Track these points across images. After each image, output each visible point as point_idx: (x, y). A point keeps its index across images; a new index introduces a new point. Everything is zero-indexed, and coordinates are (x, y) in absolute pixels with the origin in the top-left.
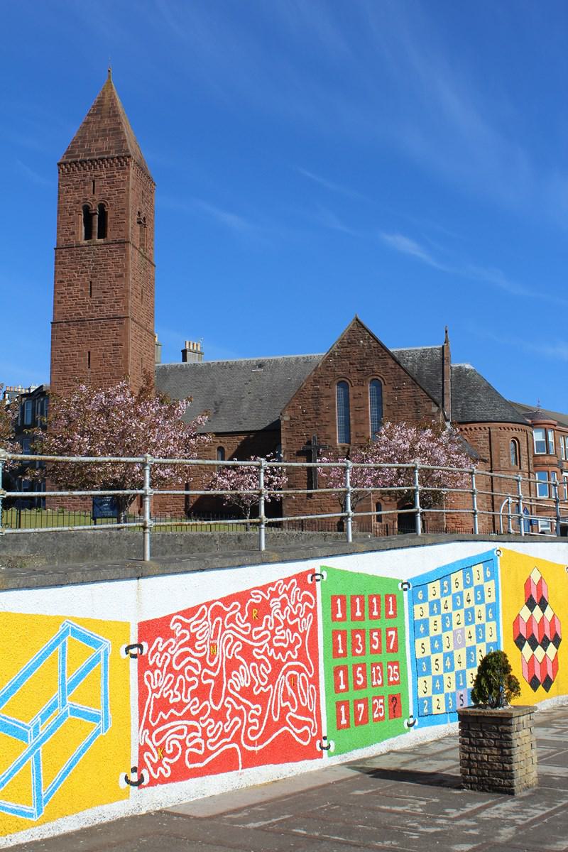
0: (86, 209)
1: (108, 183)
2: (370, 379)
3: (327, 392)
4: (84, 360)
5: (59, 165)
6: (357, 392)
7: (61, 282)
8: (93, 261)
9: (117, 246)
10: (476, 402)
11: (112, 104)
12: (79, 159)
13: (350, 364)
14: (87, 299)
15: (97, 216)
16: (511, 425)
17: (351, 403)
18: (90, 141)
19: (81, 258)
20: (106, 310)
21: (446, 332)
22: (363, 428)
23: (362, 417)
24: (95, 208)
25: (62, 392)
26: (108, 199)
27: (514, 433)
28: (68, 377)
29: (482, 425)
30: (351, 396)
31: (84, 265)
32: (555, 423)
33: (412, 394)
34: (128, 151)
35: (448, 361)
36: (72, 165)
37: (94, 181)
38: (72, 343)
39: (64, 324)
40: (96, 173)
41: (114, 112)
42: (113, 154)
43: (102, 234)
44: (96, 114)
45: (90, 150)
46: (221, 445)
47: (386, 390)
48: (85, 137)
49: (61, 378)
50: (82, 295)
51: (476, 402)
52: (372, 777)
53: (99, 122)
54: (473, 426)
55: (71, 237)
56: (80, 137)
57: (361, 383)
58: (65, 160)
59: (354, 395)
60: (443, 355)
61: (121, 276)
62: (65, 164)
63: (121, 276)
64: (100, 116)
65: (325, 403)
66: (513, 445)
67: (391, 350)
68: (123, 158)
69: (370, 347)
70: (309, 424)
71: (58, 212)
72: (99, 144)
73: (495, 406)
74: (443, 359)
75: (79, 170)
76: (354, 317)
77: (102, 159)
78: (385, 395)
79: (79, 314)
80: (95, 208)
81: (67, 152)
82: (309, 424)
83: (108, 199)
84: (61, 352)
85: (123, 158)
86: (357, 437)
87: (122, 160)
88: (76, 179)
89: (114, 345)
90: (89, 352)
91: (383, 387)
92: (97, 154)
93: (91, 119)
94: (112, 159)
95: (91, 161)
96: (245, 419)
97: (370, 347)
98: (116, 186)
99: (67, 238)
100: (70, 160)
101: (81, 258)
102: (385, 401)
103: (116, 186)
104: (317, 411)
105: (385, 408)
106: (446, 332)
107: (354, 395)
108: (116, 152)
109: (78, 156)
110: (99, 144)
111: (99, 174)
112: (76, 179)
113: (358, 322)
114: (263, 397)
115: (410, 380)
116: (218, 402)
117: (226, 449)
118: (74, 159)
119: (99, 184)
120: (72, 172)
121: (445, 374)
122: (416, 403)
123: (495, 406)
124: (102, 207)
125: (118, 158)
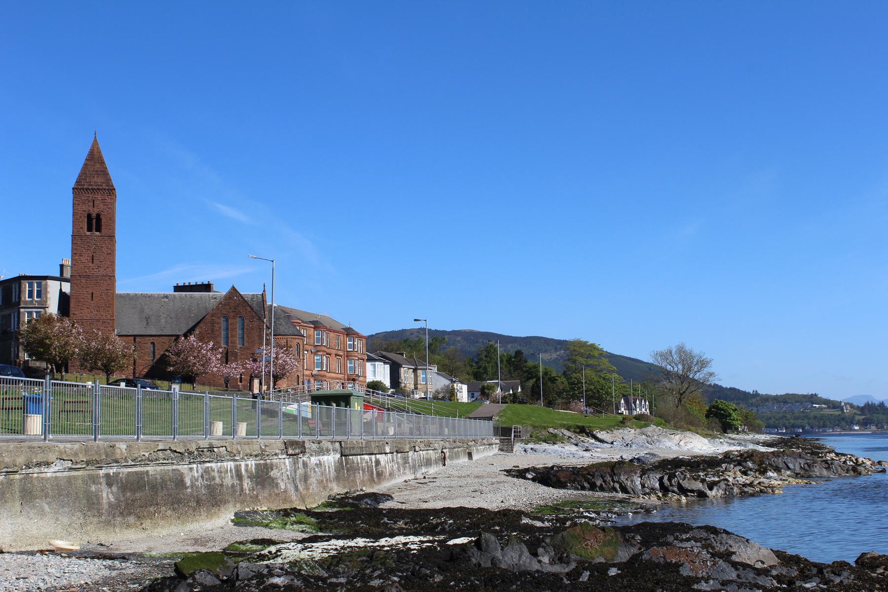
0: (89, 216)
1: (102, 203)
2: (239, 316)
3: (218, 321)
4: (89, 296)
5: (73, 189)
6: (232, 321)
7: (76, 254)
8: (94, 244)
9: (108, 237)
10: (280, 324)
11: (100, 155)
12: (85, 187)
13: (230, 308)
14: (91, 265)
15: (95, 220)
16: (297, 337)
17: (229, 327)
18: (90, 177)
19: (87, 242)
20: (102, 272)
21: (264, 286)
22: (235, 339)
23: (234, 333)
24: (94, 215)
25: (77, 312)
26: (102, 211)
27: (298, 341)
28: (81, 305)
29: (284, 337)
30: (229, 324)
31: (88, 246)
32: (300, 322)
33: (258, 324)
34: (113, 186)
35: (266, 302)
36: (79, 189)
37: (94, 201)
38: (83, 287)
39: (78, 277)
40: (95, 196)
41: (101, 160)
42: (104, 186)
43: (99, 229)
44: (91, 160)
45: (90, 183)
46: (153, 341)
47: (246, 322)
48: (86, 174)
49: (76, 305)
50: (88, 262)
51: (280, 324)
52: (388, 497)
53: (93, 165)
54: (279, 337)
55: (81, 230)
56: (84, 173)
57: (234, 317)
58: (76, 186)
59: (231, 323)
60: (263, 299)
61: (110, 254)
62: (77, 189)
63: (110, 254)
64: (93, 161)
65: (217, 326)
66: (296, 346)
67: (241, 293)
68: (111, 190)
69: (239, 300)
70: (209, 336)
71: (73, 215)
72: (95, 179)
73: (289, 327)
74: (263, 301)
75: (85, 193)
76: (232, 286)
77: (98, 189)
78: (245, 324)
79: (86, 272)
80: (94, 215)
81: (77, 182)
82: (209, 336)
83: (102, 211)
84: (76, 291)
85: (111, 190)
86: (232, 343)
87: (110, 191)
88: (83, 198)
89: (106, 290)
90: (92, 293)
91: (245, 320)
92: (96, 186)
93: (89, 163)
94: (105, 190)
95: (92, 189)
96: (164, 328)
97: (239, 300)
98: (107, 205)
99: (78, 230)
100: (80, 187)
101: (87, 242)
102: (245, 327)
103: (107, 205)
104: (213, 330)
105: (245, 330)
106: (264, 286)
107: (231, 323)
108: (106, 186)
109: (84, 185)
110: (95, 179)
111: (97, 197)
112: (83, 198)
113: (234, 288)
114: (171, 316)
115: (258, 317)
116: (147, 317)
117: (156, 343)
118: (82, 187)
119: (96, 203)
120: (81, 194)
121: (265, 310)
122: (260, 329)
123: (289, 327)
124: (98, 216)
125: (108, 189)
